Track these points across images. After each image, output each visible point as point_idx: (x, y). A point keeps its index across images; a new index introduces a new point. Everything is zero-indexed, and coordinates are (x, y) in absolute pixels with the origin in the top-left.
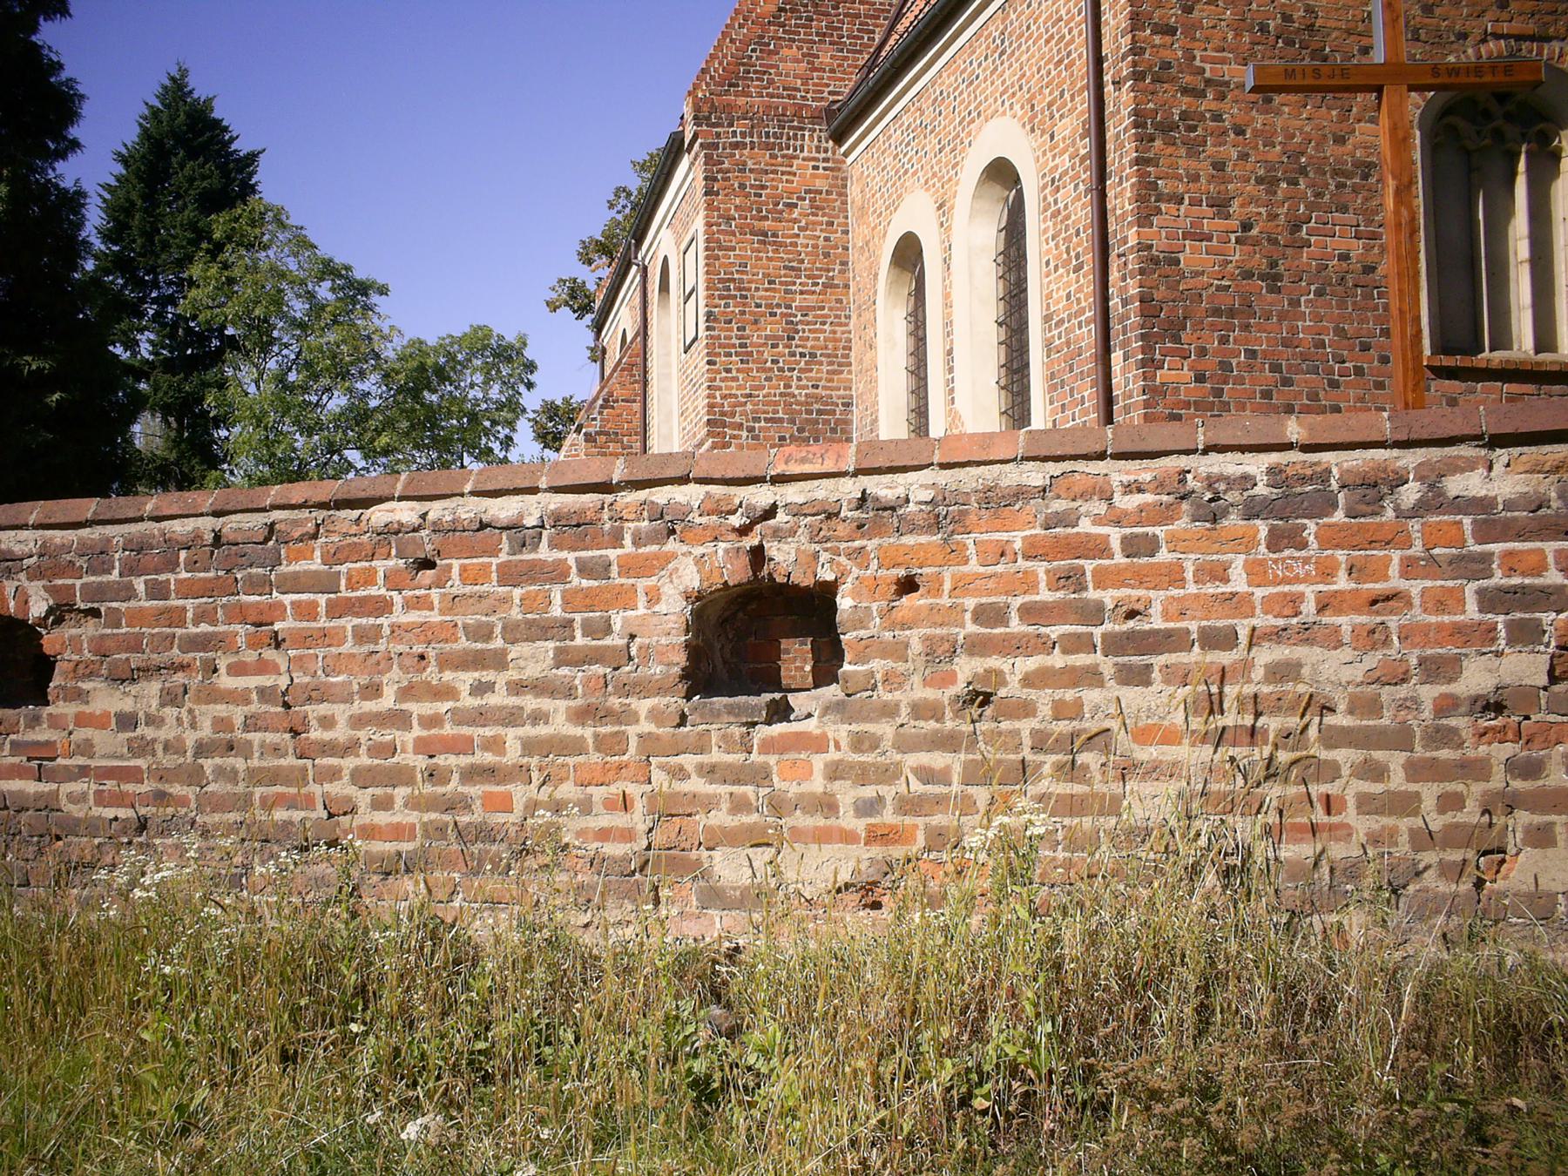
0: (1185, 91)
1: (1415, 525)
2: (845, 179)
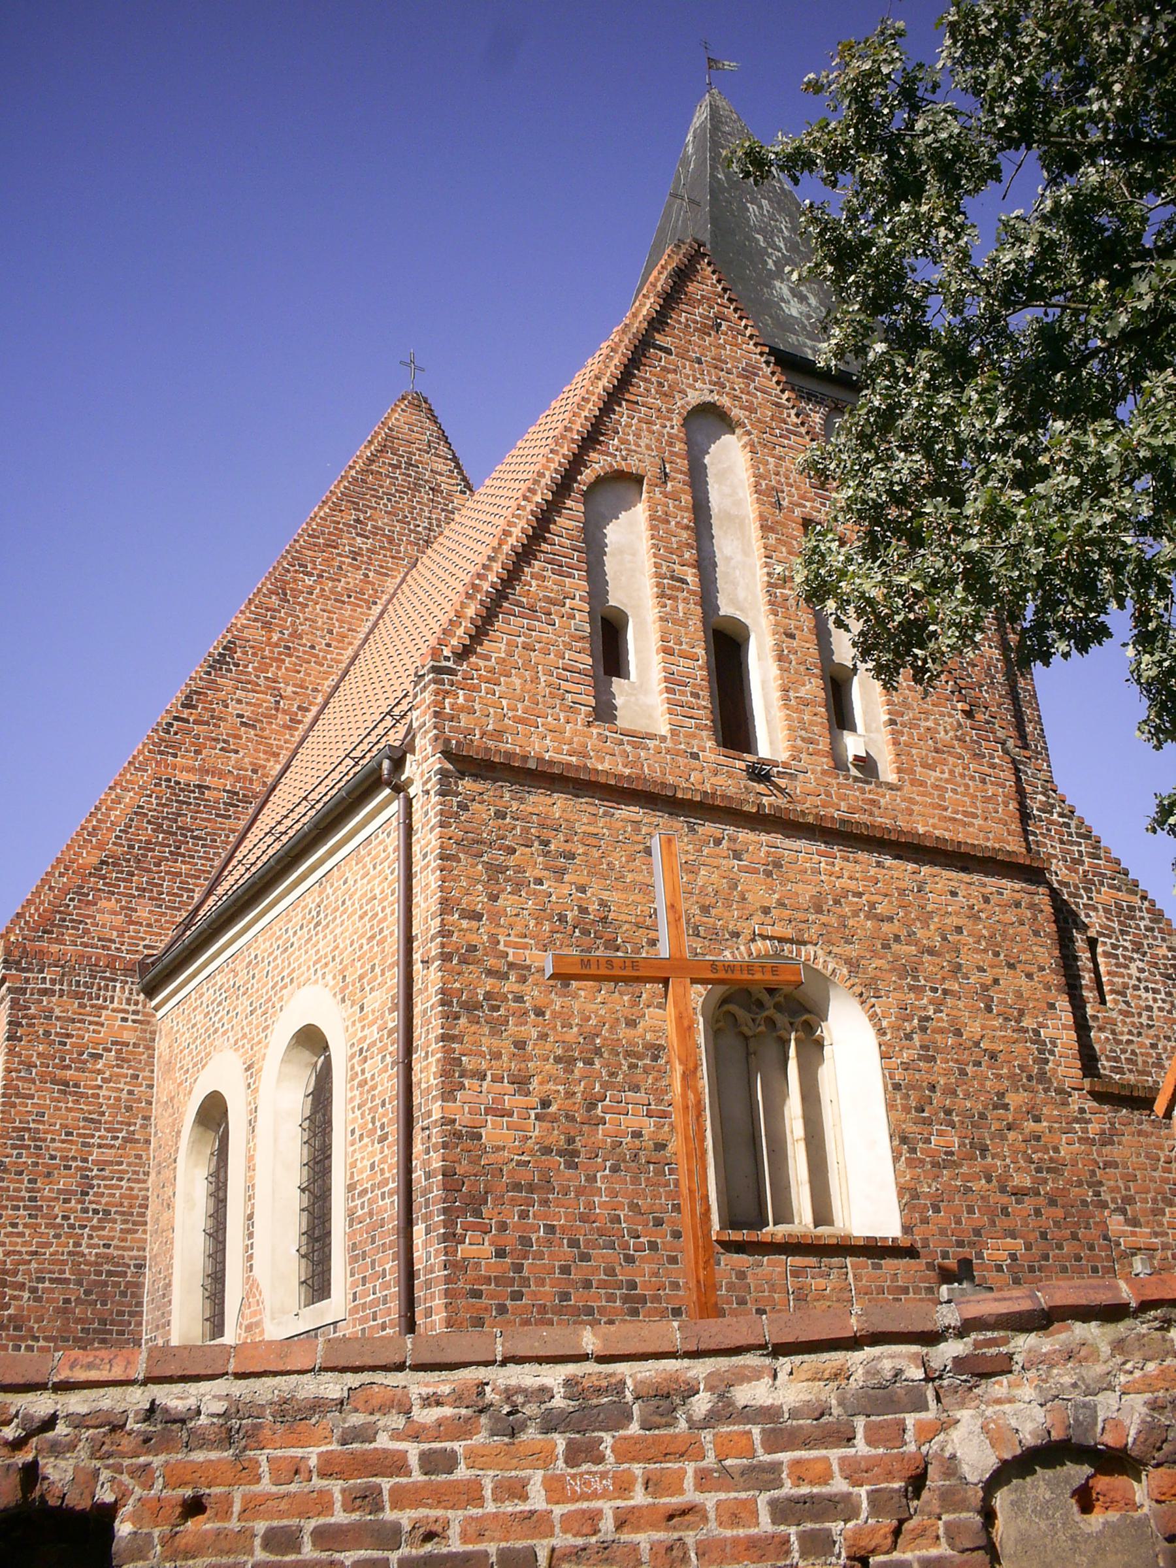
0: (490, 973)
1: (707, 1436)
2: (154, 1032)
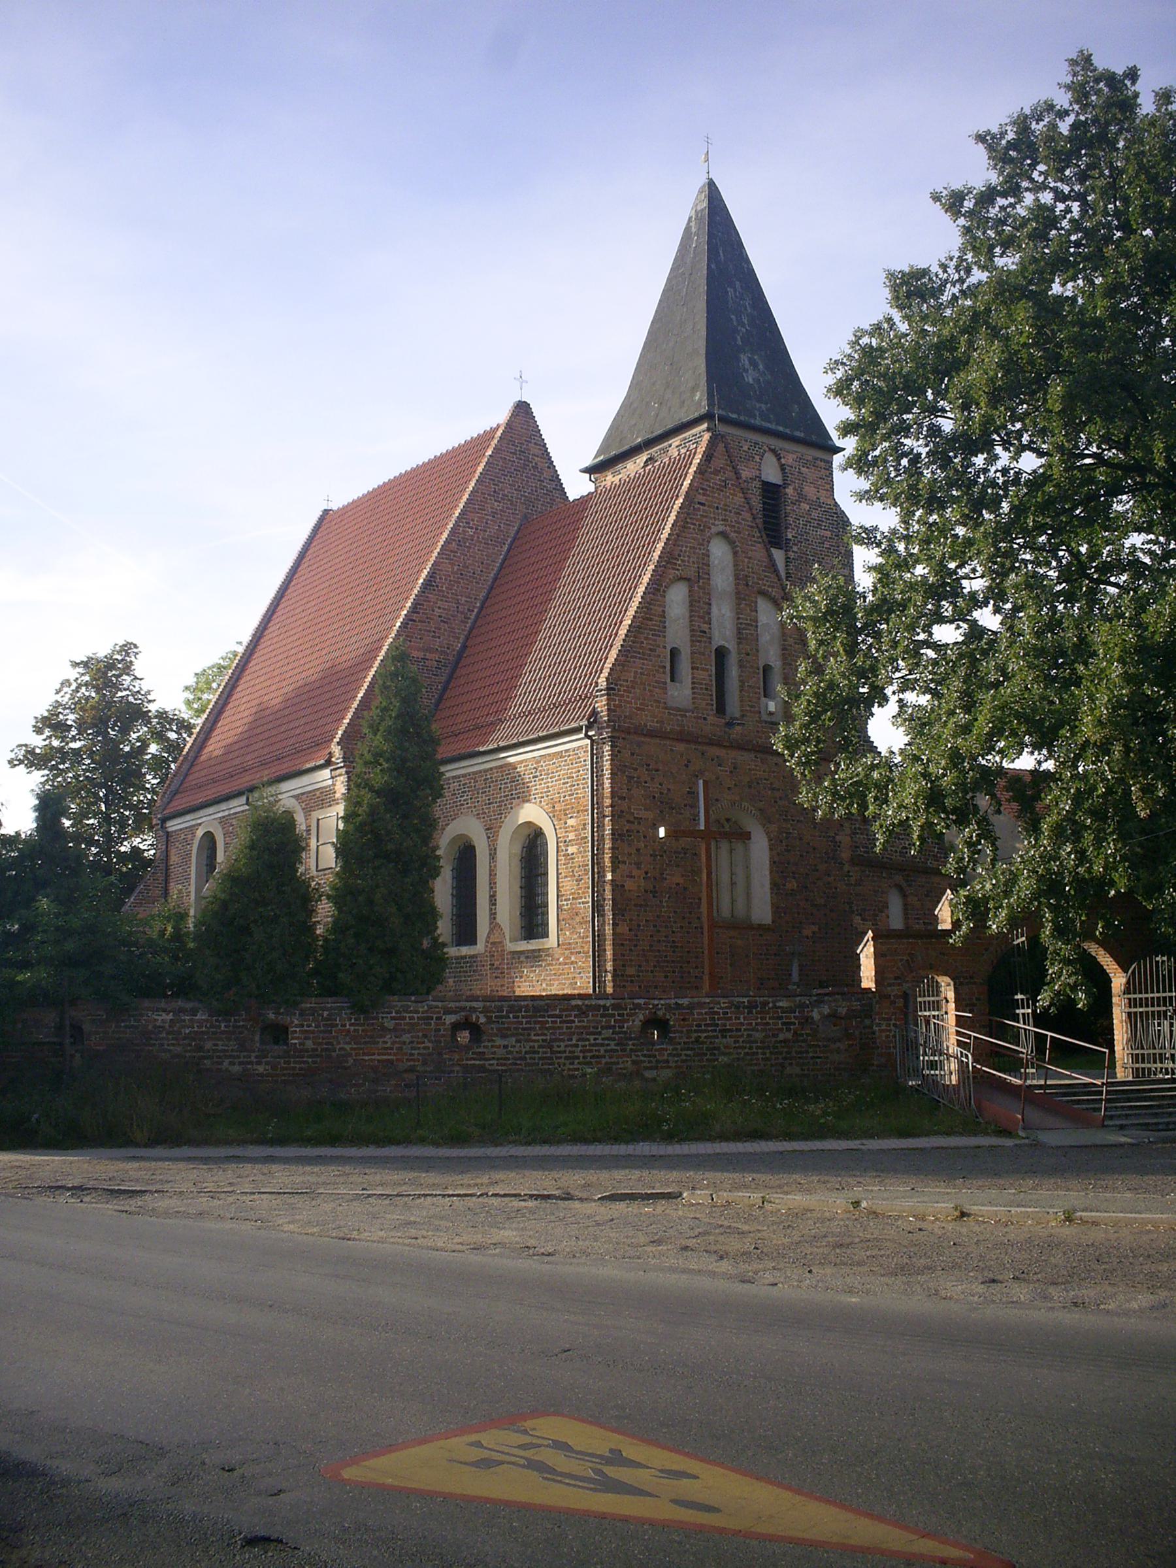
0: (628, 821)
